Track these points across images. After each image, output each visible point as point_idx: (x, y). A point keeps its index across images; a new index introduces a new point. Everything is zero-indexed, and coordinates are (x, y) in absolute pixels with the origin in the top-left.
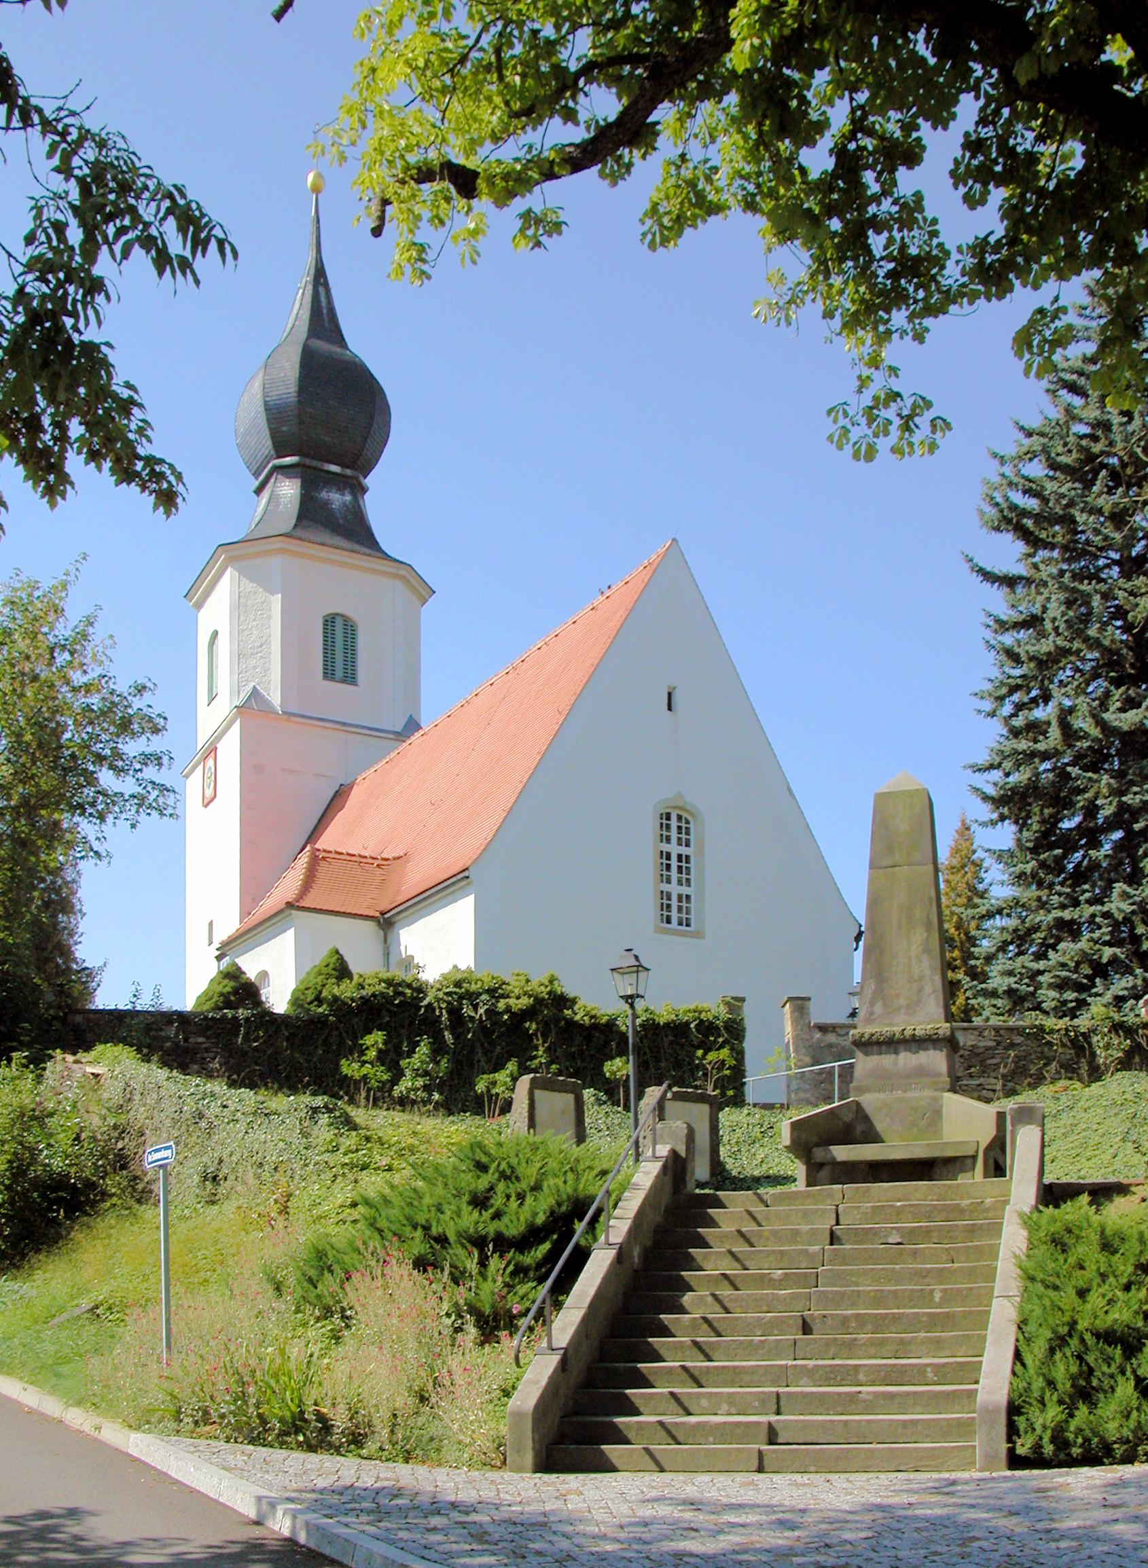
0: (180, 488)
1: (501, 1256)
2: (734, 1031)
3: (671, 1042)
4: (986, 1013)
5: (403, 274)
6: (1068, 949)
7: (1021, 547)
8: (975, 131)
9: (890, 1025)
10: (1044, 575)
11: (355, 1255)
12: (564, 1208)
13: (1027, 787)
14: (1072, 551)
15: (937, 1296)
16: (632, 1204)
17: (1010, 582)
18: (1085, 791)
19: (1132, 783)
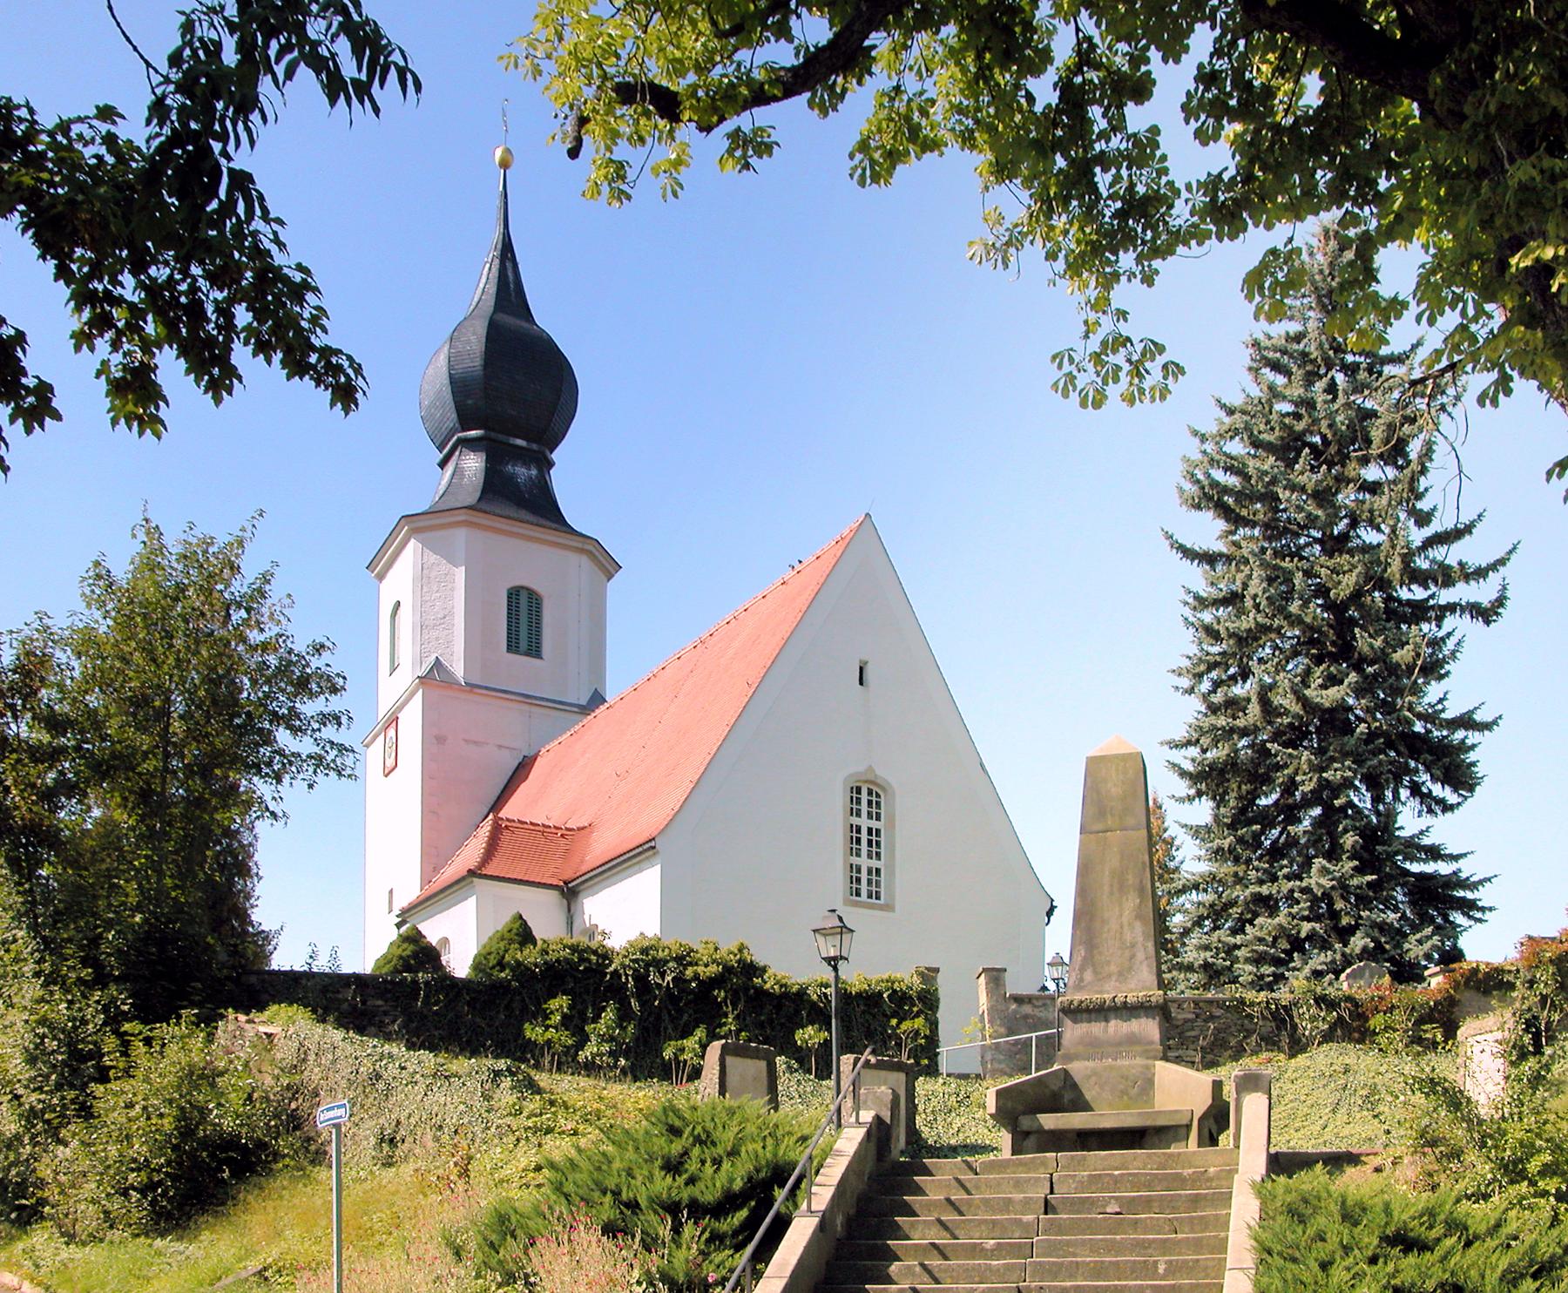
0: (360, 382)
1: (696, 1223)
2: (928, 1001)
3: (863, 1012)
4: (1181, 987)
5: (599, 193)
6: (1265, 924)
7: (1221, 525)
8: (1210, 63)
9: (1101, 992)
10: (1245, 552)
11: (540, 1221)
12: (762, 1175)
13: (1226, 763)
14: (1273, 529)
15: (1161, 1269)
16: (834, 1172)
17: (1209, 559)
18: (1286, 766)
19: (1333, 759)
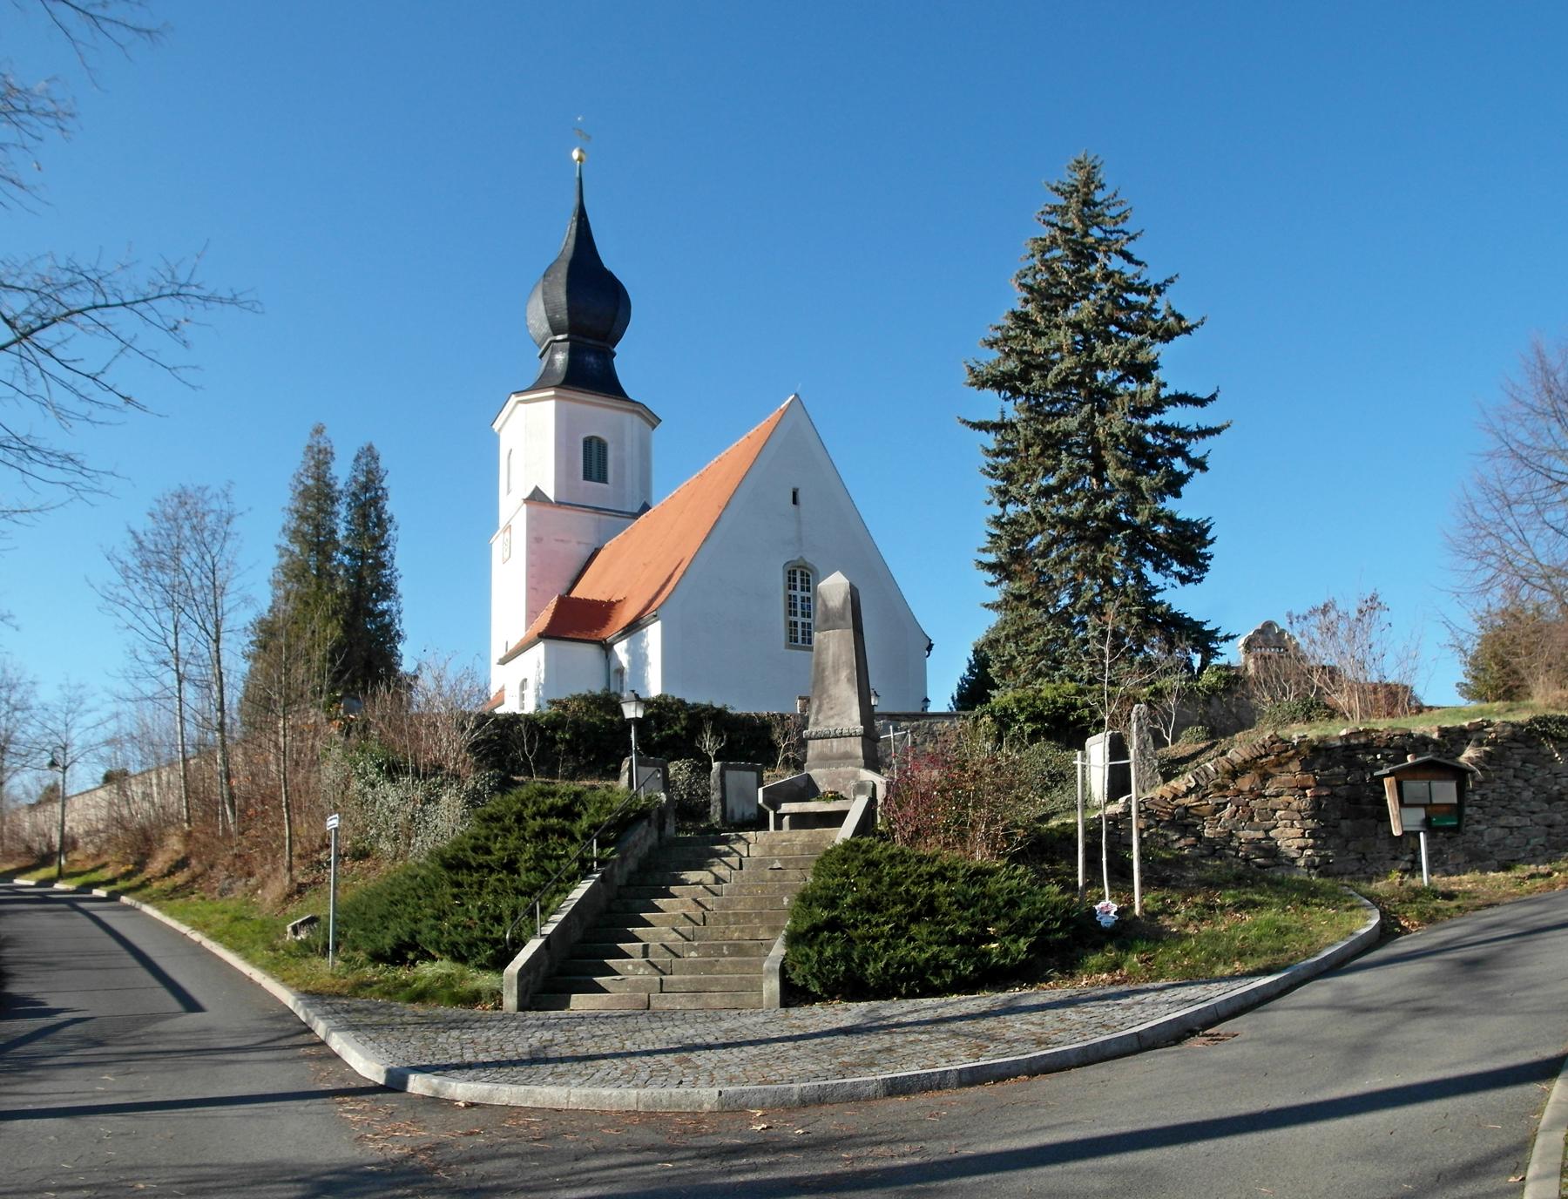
17: (997, 427)
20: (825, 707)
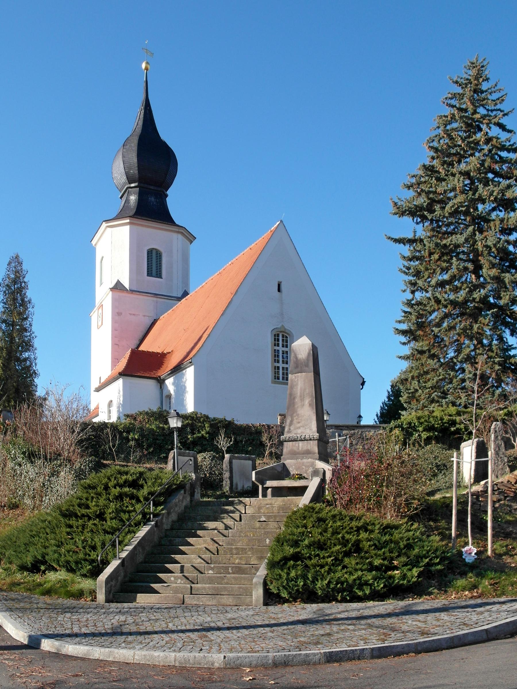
17: (411, 241)
20: (295, 421)
